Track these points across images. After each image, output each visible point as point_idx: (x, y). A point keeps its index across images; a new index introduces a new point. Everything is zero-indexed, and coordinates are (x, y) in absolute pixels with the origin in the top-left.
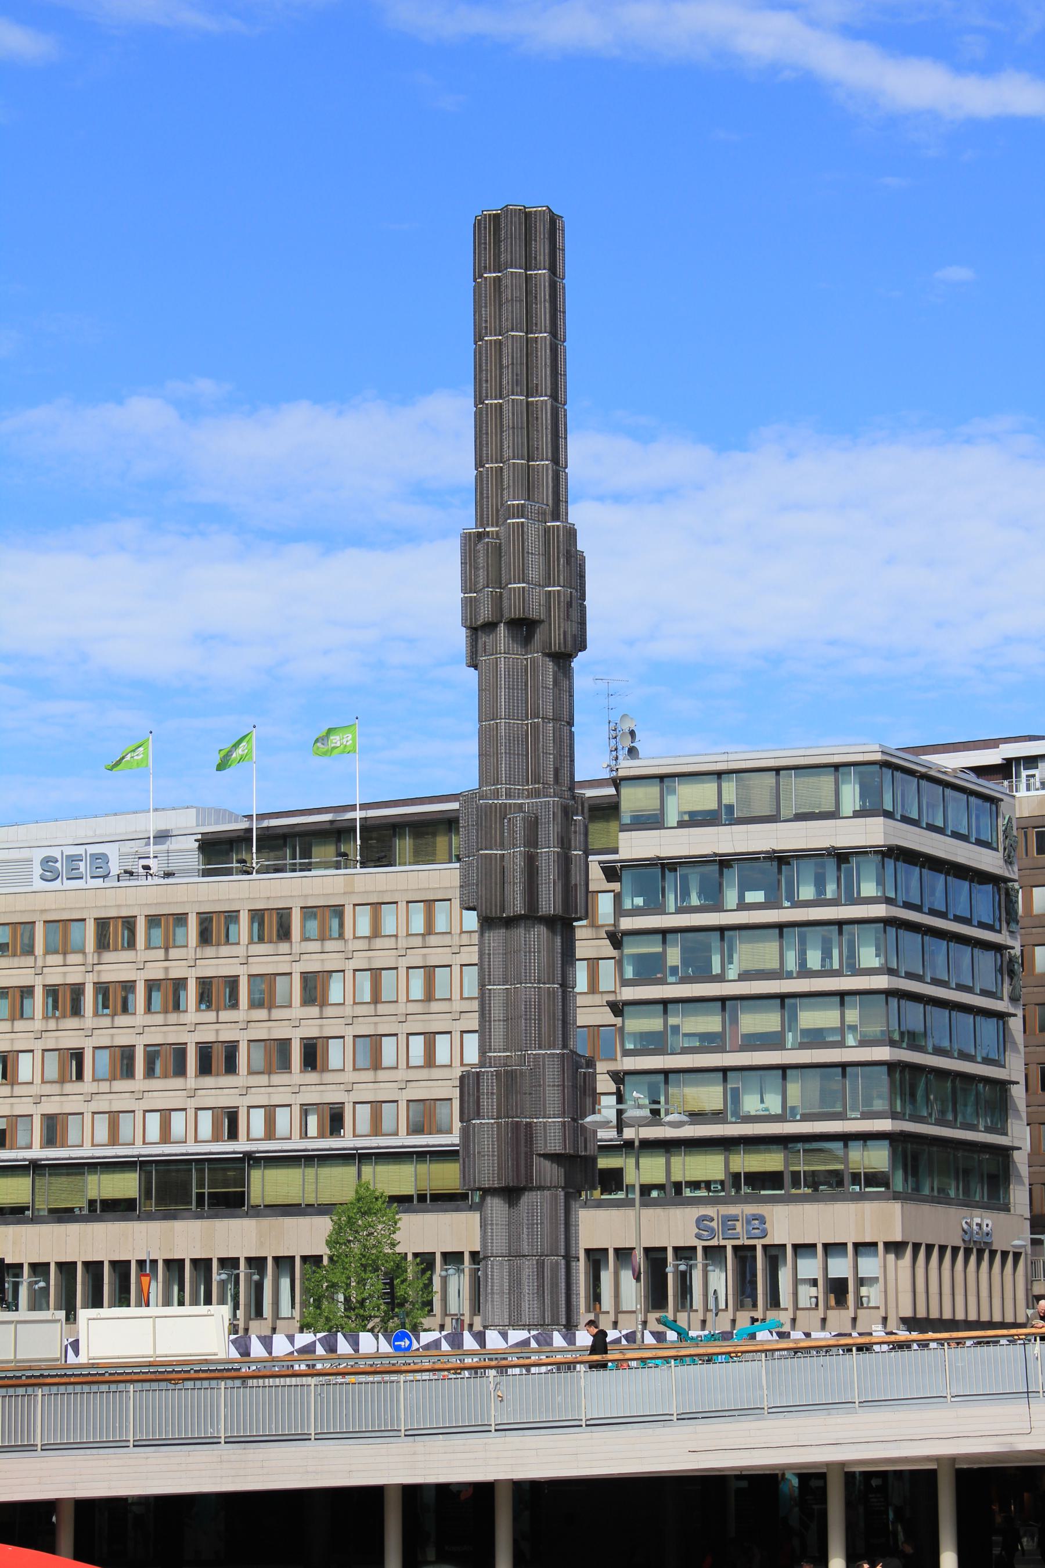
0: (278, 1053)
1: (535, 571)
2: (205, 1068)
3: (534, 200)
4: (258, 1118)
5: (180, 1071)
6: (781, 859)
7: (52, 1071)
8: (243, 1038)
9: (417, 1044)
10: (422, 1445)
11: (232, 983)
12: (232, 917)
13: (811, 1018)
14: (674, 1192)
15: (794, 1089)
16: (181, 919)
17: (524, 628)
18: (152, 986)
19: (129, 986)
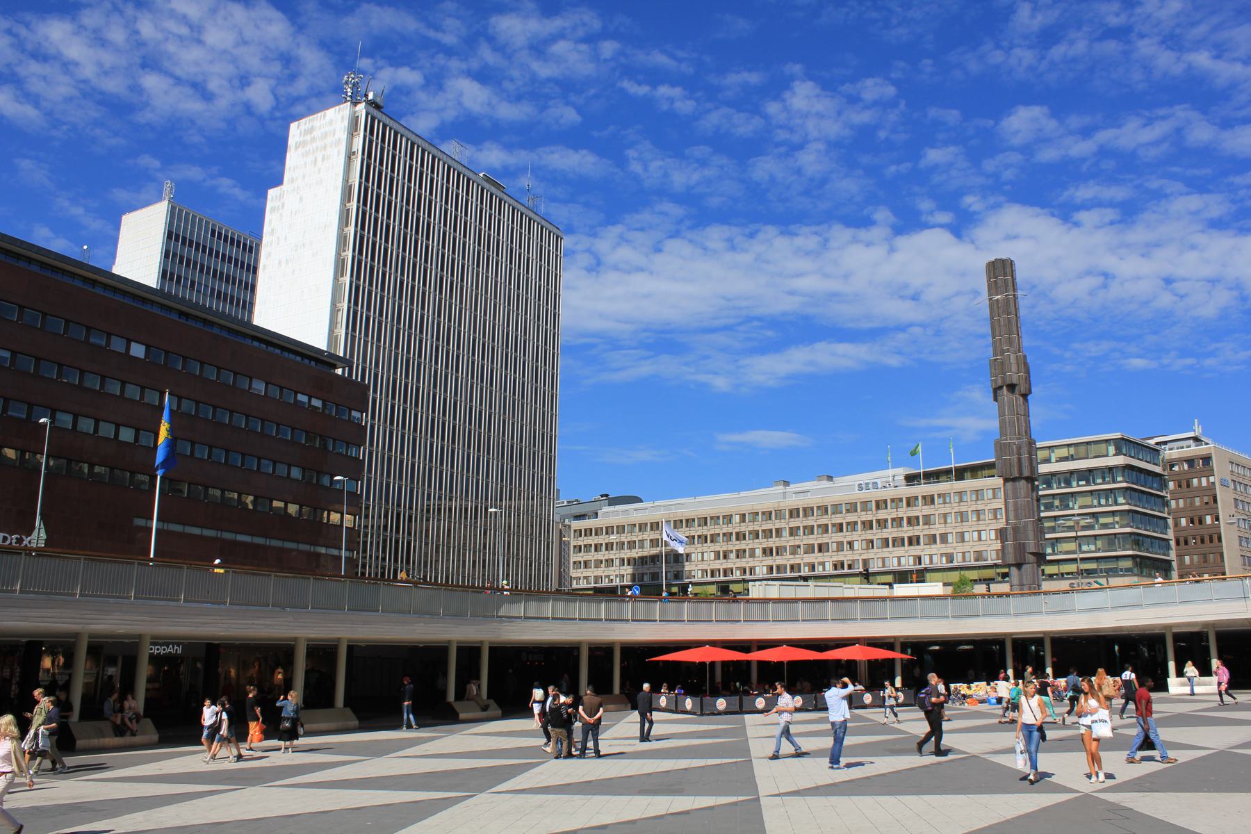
1: (1014, 369)
2: (910, 544)
3: (1004, 257)
4: (927, 558)
5: (903, 545)
7: (864, 546)
8: (921, 534)
9: (976, 534)
10: (1052, 617)
11: (917, 518)
12: (916, 498)
13: (1102, 520)
14: (1061, 576)
15: (1099, 543)
16: (901, 500)
17: (1011, 387)
18: (893, 520)
19: (886, 520)
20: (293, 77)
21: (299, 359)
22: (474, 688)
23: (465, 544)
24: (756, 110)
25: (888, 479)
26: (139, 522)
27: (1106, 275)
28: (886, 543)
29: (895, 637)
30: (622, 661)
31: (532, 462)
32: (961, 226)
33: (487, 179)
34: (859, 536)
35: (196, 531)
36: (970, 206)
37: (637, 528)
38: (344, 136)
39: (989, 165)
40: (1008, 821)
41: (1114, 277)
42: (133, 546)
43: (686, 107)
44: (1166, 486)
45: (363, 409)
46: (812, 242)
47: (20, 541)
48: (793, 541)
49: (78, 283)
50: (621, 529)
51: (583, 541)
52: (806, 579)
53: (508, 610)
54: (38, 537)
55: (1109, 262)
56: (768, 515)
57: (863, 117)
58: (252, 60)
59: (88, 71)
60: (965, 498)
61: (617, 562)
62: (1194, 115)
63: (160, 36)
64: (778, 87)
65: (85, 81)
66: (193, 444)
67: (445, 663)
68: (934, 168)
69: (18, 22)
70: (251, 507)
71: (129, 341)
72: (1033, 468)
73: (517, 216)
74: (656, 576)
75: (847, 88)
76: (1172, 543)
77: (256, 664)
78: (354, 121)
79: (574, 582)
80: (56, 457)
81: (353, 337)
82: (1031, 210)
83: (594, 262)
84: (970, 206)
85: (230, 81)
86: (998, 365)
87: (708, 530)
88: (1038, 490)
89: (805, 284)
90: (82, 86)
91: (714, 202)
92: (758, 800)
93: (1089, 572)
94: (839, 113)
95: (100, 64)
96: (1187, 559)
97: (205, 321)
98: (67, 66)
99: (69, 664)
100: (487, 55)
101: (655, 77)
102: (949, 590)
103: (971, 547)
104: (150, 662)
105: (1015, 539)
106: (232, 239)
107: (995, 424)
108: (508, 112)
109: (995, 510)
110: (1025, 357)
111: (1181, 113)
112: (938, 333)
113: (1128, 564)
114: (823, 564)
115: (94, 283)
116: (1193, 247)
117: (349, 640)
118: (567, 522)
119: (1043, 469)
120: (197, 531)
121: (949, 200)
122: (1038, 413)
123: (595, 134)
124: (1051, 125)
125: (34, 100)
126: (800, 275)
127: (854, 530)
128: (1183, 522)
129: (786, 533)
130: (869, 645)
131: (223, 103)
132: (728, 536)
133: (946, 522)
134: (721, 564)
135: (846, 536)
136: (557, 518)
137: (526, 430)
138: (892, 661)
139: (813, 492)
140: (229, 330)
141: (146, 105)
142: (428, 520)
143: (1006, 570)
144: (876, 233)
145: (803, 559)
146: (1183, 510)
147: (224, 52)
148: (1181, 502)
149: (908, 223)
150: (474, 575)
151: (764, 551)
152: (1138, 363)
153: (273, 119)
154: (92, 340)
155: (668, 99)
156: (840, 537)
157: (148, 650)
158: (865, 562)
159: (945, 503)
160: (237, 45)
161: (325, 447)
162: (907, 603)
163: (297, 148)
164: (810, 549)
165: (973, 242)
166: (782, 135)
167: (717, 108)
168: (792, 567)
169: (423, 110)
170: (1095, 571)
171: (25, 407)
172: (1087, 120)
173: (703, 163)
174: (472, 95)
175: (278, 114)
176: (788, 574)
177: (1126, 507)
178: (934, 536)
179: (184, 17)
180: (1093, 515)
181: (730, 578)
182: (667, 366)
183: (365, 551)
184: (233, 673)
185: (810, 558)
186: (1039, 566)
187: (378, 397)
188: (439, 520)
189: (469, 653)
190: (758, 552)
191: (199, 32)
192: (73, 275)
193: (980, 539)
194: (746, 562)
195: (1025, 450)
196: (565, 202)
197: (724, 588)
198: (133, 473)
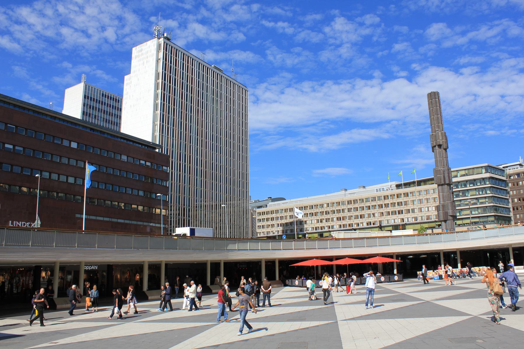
0: (408, 211)
1: (440, 138)
2: (399, 213)
3: (435, 91)
4: (406, 219)
6: (475, 180)
8: (403, 209)
9: (426, 208)
10: (460, 242)
11: (402, 202)
12: (401, 194)
13: (480, 201)
14: (464, 225)
15: (479, 211)
16: (394, 195)
17: (440, 146)
18: (391, 204)
20: (123, 26)
21: (140, 146)
22: (218, 279)
23: (212, 220)
24: (320, 31)
25: (388, 187)
26: (78, 216)
27: (475, 95)
28: (388, 213)
29: (393, 253)
30: (279, 267)
31: (239, 185)
32: (412, 77)
33: (216, 68)
34: (377, 211)
35: (101, 219)
36: (415, 68)
37: (324, 213)
38: (154, 52)
39: (422, 50)
40: (442, 329)
41: (479, 96)
42: (75, 226)
43: (290, 31)
44: (508, 185)
45: (168, 166)
46: (348, 87)
47: (30, 225)
48: (349, 214)
49: (49, 118)
50: (277, 212)
51: (261, 217)
52: (355, 230)
53: (230, 247)
54: (37, 223)
55: (476, 89)
56: (338, 203)
57: (366, 32)
58: (106, 19)
59: (39, 28)
60: (421, 193)
61: (276, 225)
62: (511, 23)
63: (67, 11)
64: (329, 20)
65: (38, 32)
66: (98, 183)
67: (206, 270)
68: (398, 52)
69: (8, 9)
70: (123, 208)
71: (70, 141)
72: (450, 180)
73: (232, 85)
74: (292, 231)
75: (358, 19)
76: (511, 209)
77: (128, 272)
78: (159, 46)
79: (258, 234)
80: (43, 190)
81: (162, 136)
82: (441, 69)
83: (256, 99)
84: (415, 68)
85: (97, 29)
86: (434, 137)
87: (314, 211)
88: (453, 189)
89: (345, 104)
90: (36, 34)
91: (305, 71)
92: (337, 322)
93: (476, 223)
94: (356, 30)
95: (43, 25)
96: (518, 216)
97: (101, 132)
98: (30, 26)
99: (52, 274)
100: (204, 12)
101: (276, 18)
102: (416, 232)
103: (425, 214)
104: (85, 273)
105: (443, 210)
106: (111, 97)
107: (433, 160)
108: (215, 37)
109: (435, 198)
110: (445, 133)
111: (505, 22)
112: (404, 123)
113: (492, 219)
114: (362, 223)
115: (55, 118)
116: (513, 81)
117: (166, 262)
118: (254, 209)
119: (454, 180)
120: (101, 219)
121: (405, 66)
122: (451, 154)
123: (253, 44)
124: (448, 31)
125: (18, 41)
126: (344, 101)
127: (375, 208)
128: (516, 200)
129: (346, 211)
130: (383, 256)
131: (95, 38)
132: (322, 213)
133: (414, 204)
134: (320, 225)
135: (372, 211)
136: (250, 208)
137: (236, 172)
138: (393, 263)
139: (357, 193)
140: (111, 135)
141: (64, 40)
142: (196, 211)
143: (440, 223)
144: (375, 82)
145: (354, 221)
146: (515, 195)
147: (94, 17)
148: (515, 192)
149: (388, 77)
150: (216, 232)
151: (337, 218)
152: (491, 133)
153: (117, 44)
154: (55, 141)
155: (282, 28)
156: (369, 212)
157: (84, 268)
158: (380, 222)
159: (413, 196)
160: (99, 14)
161: (153, 182)
162: (398, 238)
163: (136, 58)
164: (357, 217)
165: (417, 84)
166: (332, 41)
167: (303, 31)
168: (349, 225)
169: (179, 37)
170: (479, 222)
171: (30, 170)
172: (463, 28)
173: (299, 54)
174: (199, 30)
175: (118, 42)
176: (348, 228)
177: (491, 195)
178: (409, 210)
179: (76, 3)
180: (477, 199)
181: (323, 230)
182: (289, 142)
183: (171, 224)
184: (119, 276)
185: (357, 221)
186: (454, 221)
187: (174, 160)
188: (201, 211)
189: (215, 265)
190: (335, 219)
191: (83, 9)
192: (47, 115)
193: (428, 211)
194: (330, 224)
195: (446, 172)
196: (242, 74)
197: (321, 235)
198: (74, 196)
